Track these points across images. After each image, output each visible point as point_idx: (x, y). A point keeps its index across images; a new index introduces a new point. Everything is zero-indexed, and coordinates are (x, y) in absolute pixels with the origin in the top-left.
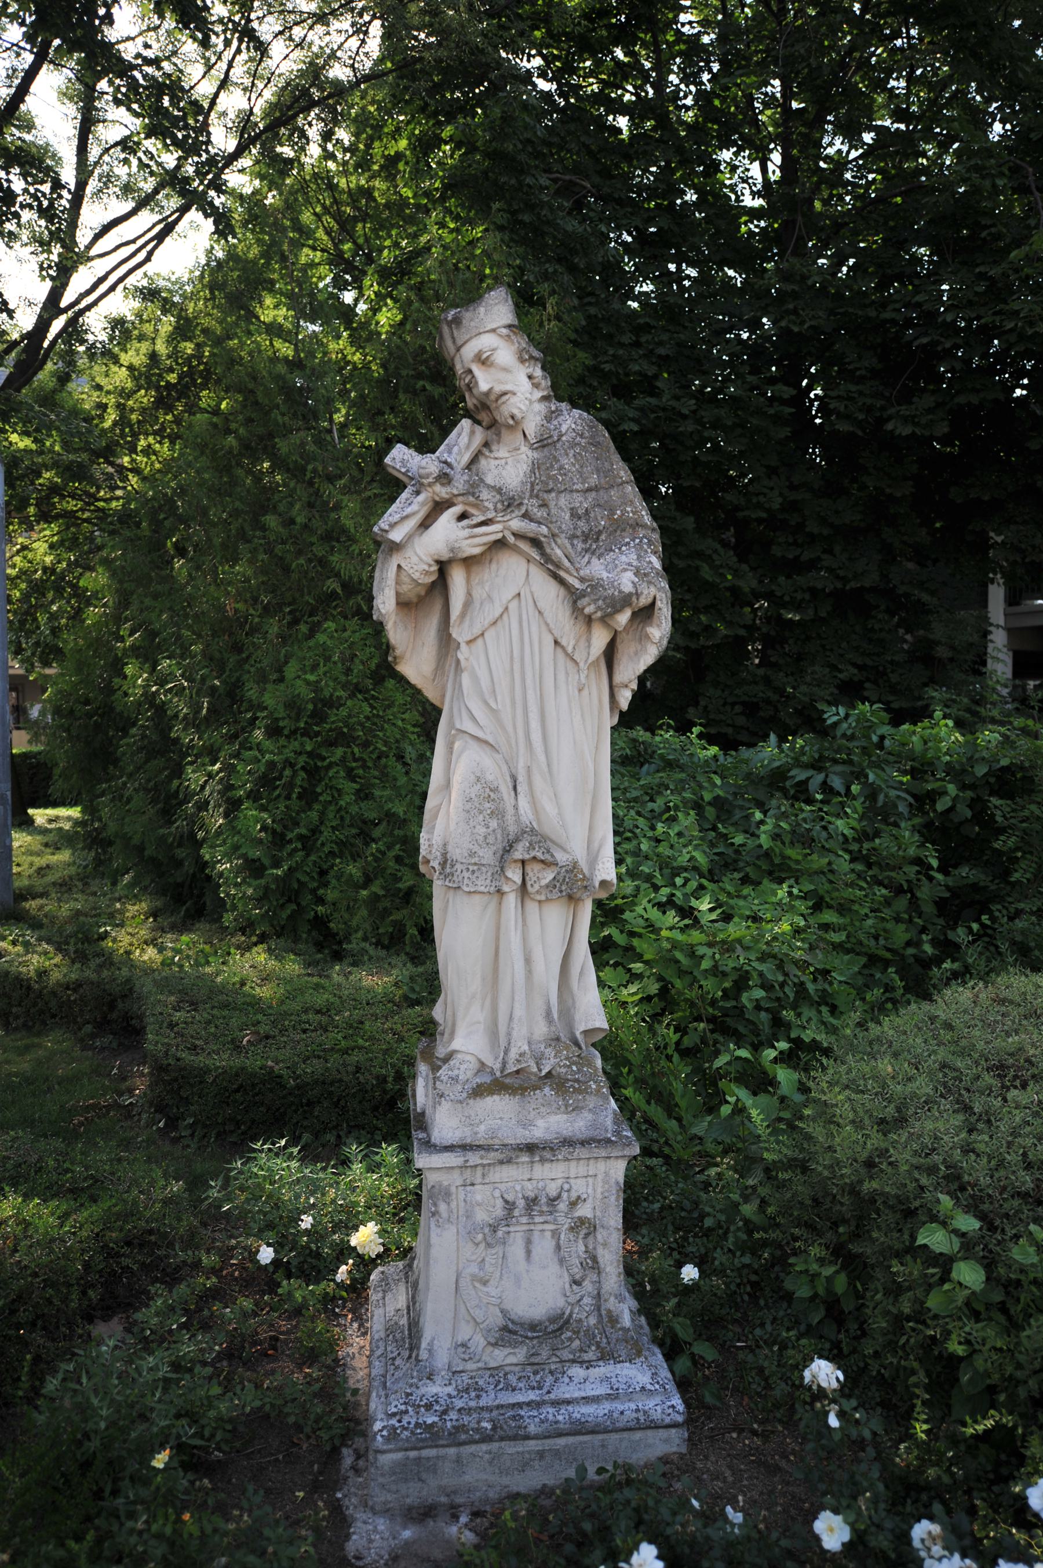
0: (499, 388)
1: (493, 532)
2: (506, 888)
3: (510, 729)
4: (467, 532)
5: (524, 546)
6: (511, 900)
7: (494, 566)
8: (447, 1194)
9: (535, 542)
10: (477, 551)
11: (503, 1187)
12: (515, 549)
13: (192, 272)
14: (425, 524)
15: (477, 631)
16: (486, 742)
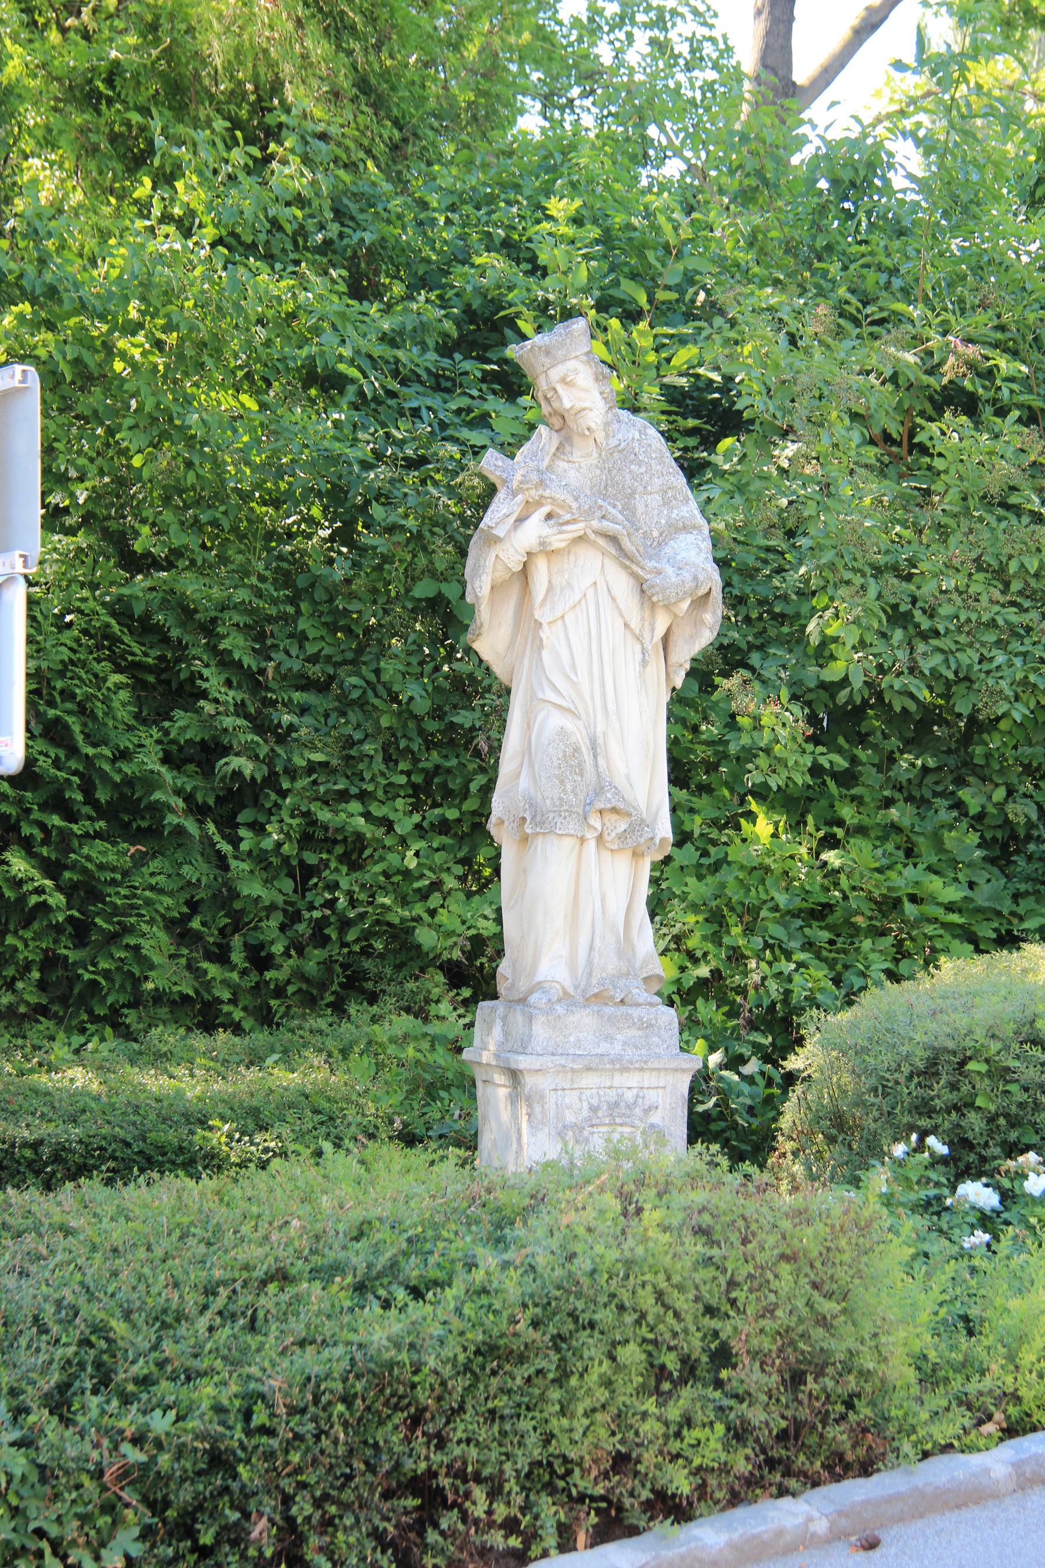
0: (579, 405)
1: (577, 529)
2: (588, 835)
3: (588, 699)
4: (555, 530)
5: (601, 541)
6: (591, 845)
7: (572, 557)
8: (542, 1097)
9: (613, 539)
10: (563, 545)
11: (588, 1093)
12: (593, 544)
13: (312, 401)
14: (521, 520)
15: (558, 614)
16: (568, 710)
